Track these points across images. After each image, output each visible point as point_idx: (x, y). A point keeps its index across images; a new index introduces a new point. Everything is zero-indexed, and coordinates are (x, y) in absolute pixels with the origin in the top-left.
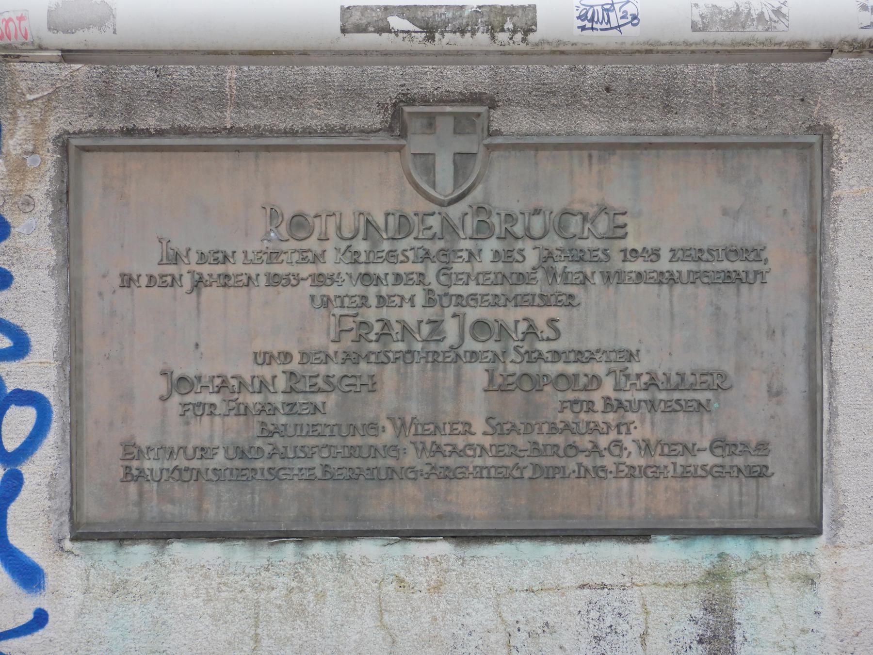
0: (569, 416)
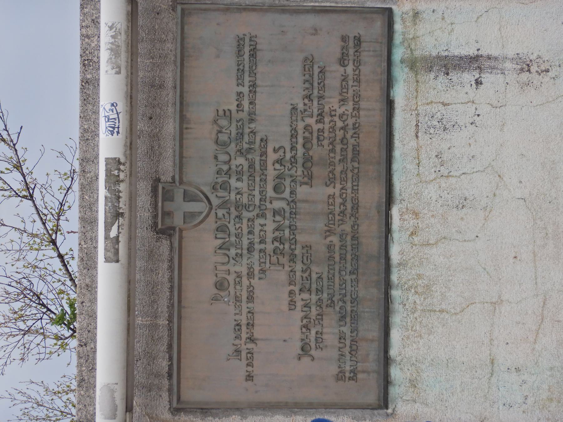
0: (326, 142)
